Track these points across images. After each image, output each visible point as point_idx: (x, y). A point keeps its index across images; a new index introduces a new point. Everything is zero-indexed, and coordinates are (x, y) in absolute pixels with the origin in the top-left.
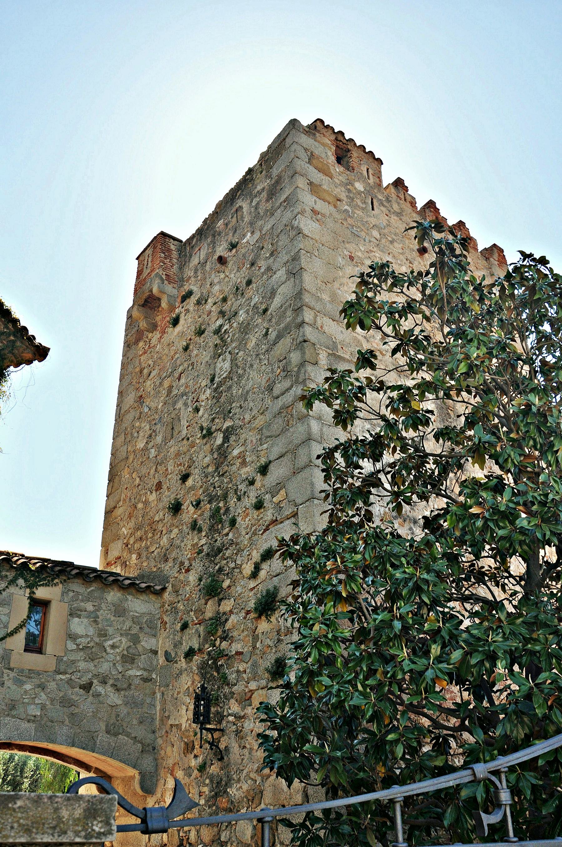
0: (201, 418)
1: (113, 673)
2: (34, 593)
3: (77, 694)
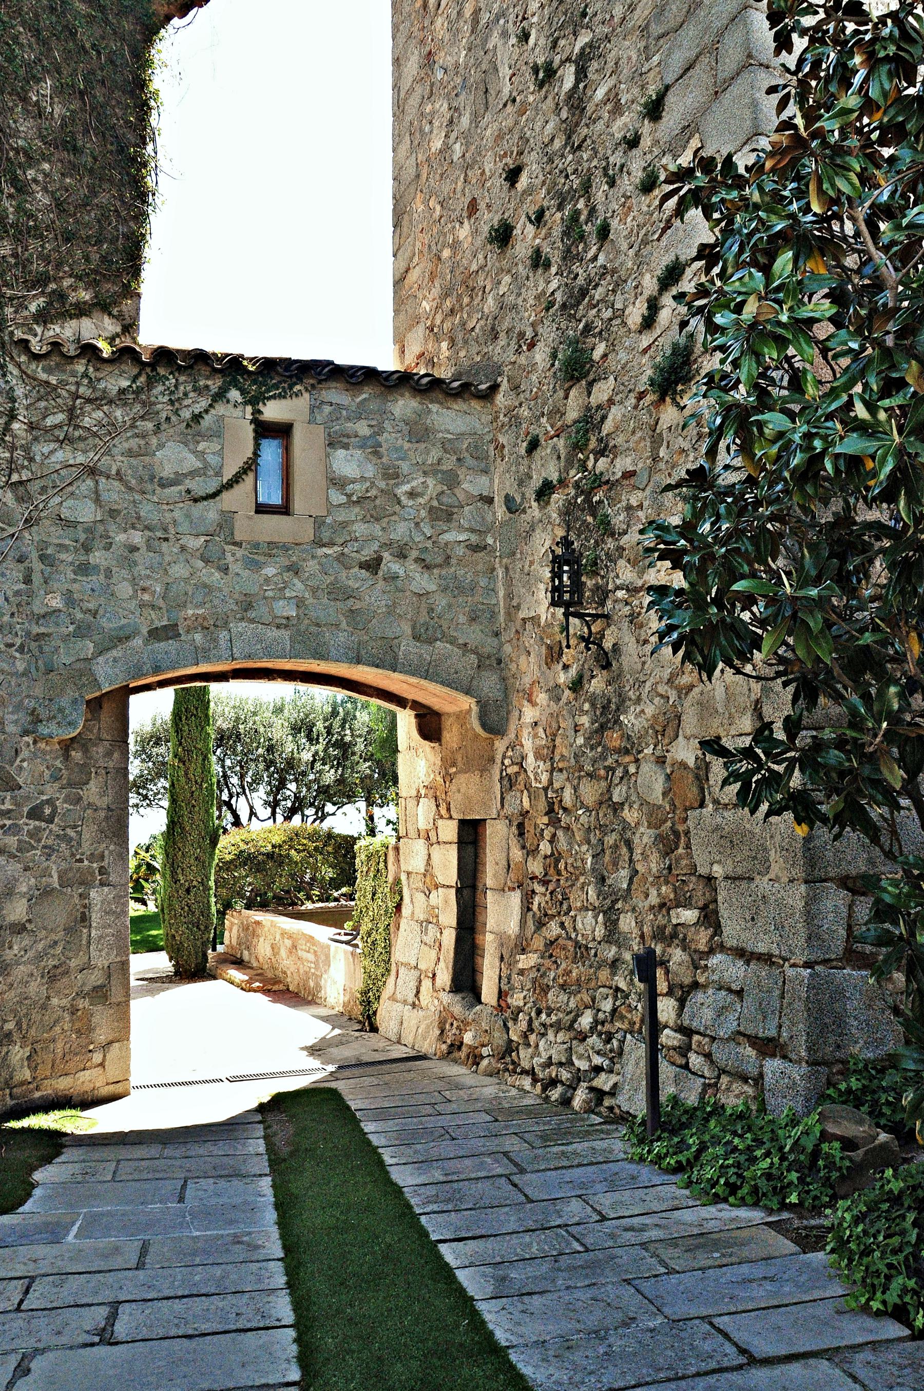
0: (533, 49)
1: (417, 540)
2: (260, 412)
3: (356, 579)
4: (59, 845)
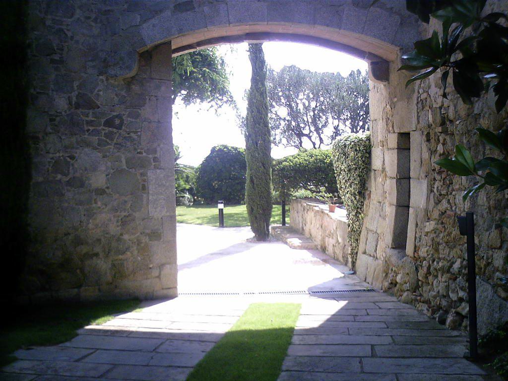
4: (125, 143)
